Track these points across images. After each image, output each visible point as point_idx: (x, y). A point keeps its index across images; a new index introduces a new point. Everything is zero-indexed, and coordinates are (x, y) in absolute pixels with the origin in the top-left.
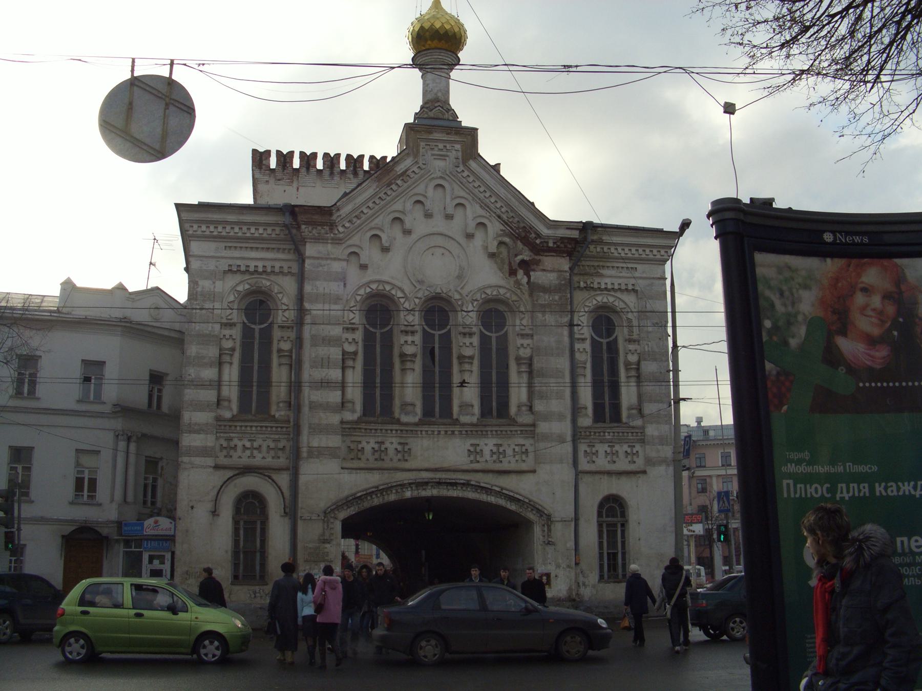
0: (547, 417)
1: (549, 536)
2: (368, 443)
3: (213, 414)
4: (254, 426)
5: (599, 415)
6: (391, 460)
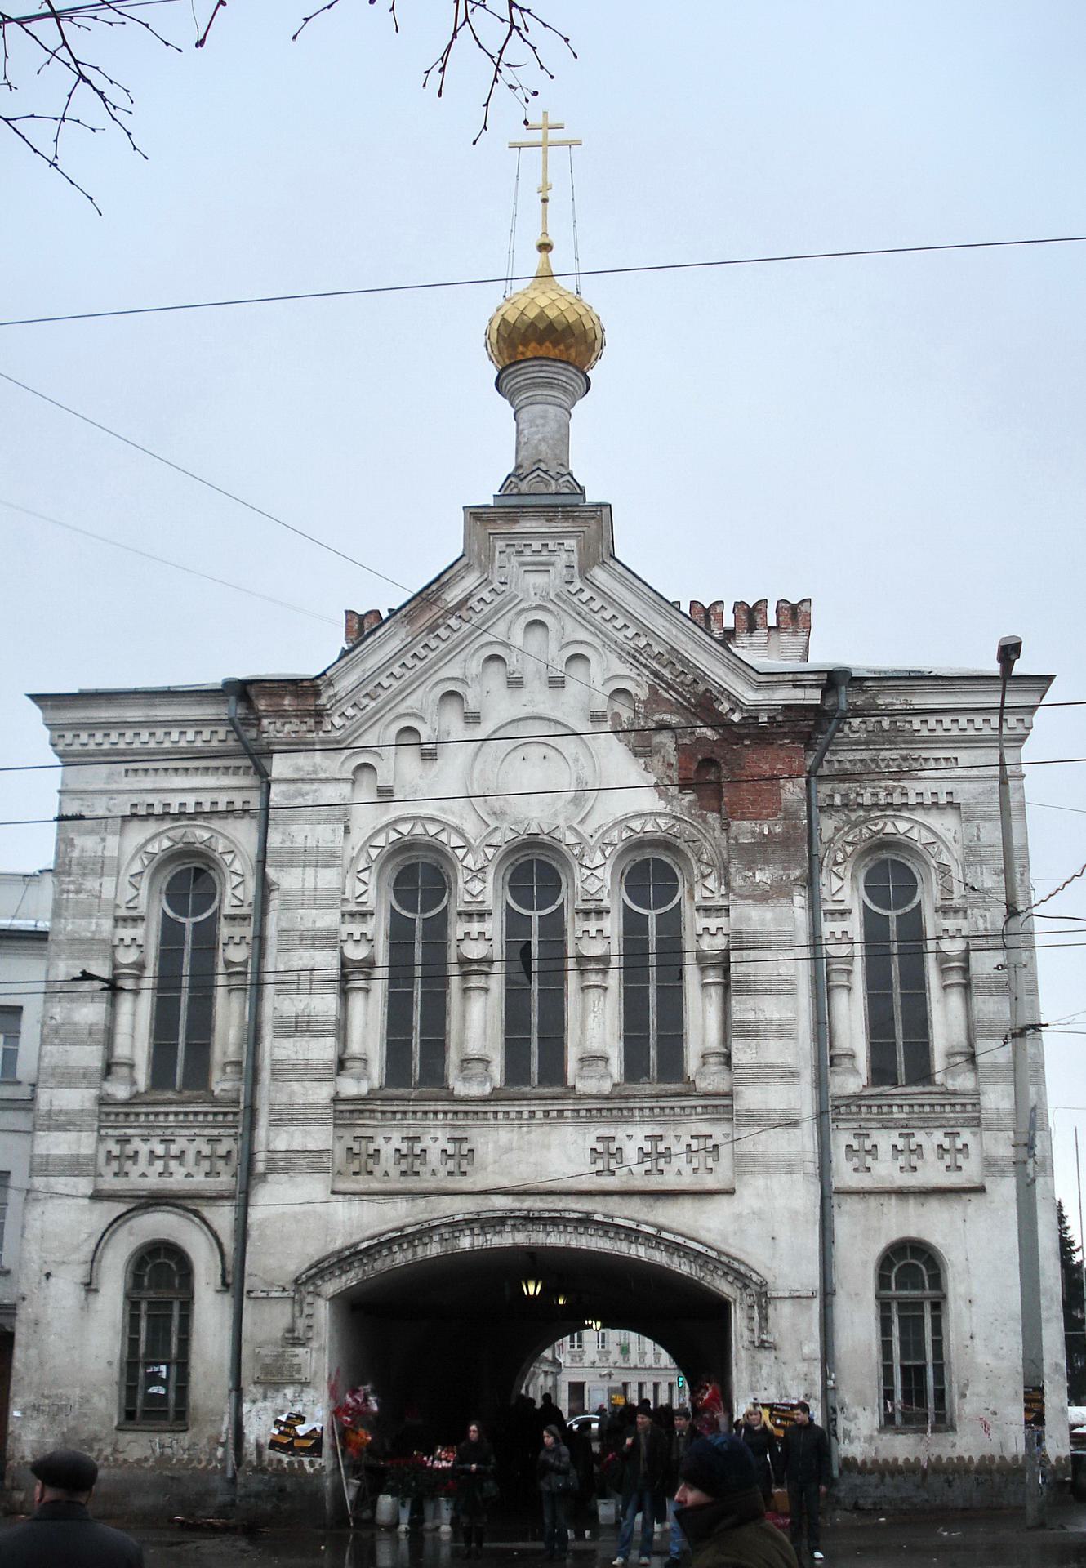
0: (760, 1076)
1: (762, 1330)
2: (388, 1139)
3: (94, 1092)
4: (171, 1113)
5: (881, 1072)
6: (434, 1173)
